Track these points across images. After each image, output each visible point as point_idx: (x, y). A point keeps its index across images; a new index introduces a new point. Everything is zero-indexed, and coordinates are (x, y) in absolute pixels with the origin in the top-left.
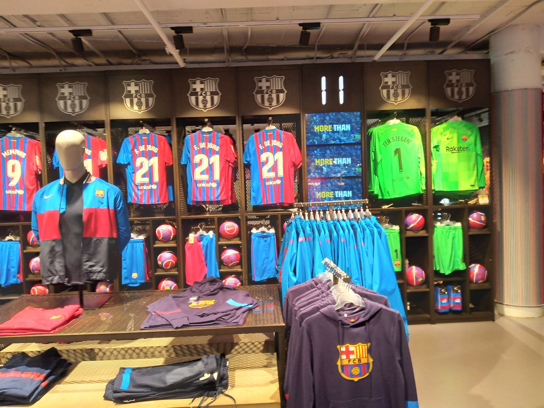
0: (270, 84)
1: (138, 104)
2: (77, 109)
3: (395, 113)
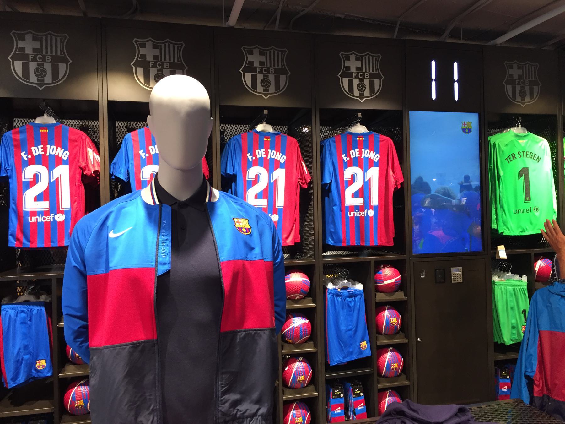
2: (48, 79)
3: (266, 112)
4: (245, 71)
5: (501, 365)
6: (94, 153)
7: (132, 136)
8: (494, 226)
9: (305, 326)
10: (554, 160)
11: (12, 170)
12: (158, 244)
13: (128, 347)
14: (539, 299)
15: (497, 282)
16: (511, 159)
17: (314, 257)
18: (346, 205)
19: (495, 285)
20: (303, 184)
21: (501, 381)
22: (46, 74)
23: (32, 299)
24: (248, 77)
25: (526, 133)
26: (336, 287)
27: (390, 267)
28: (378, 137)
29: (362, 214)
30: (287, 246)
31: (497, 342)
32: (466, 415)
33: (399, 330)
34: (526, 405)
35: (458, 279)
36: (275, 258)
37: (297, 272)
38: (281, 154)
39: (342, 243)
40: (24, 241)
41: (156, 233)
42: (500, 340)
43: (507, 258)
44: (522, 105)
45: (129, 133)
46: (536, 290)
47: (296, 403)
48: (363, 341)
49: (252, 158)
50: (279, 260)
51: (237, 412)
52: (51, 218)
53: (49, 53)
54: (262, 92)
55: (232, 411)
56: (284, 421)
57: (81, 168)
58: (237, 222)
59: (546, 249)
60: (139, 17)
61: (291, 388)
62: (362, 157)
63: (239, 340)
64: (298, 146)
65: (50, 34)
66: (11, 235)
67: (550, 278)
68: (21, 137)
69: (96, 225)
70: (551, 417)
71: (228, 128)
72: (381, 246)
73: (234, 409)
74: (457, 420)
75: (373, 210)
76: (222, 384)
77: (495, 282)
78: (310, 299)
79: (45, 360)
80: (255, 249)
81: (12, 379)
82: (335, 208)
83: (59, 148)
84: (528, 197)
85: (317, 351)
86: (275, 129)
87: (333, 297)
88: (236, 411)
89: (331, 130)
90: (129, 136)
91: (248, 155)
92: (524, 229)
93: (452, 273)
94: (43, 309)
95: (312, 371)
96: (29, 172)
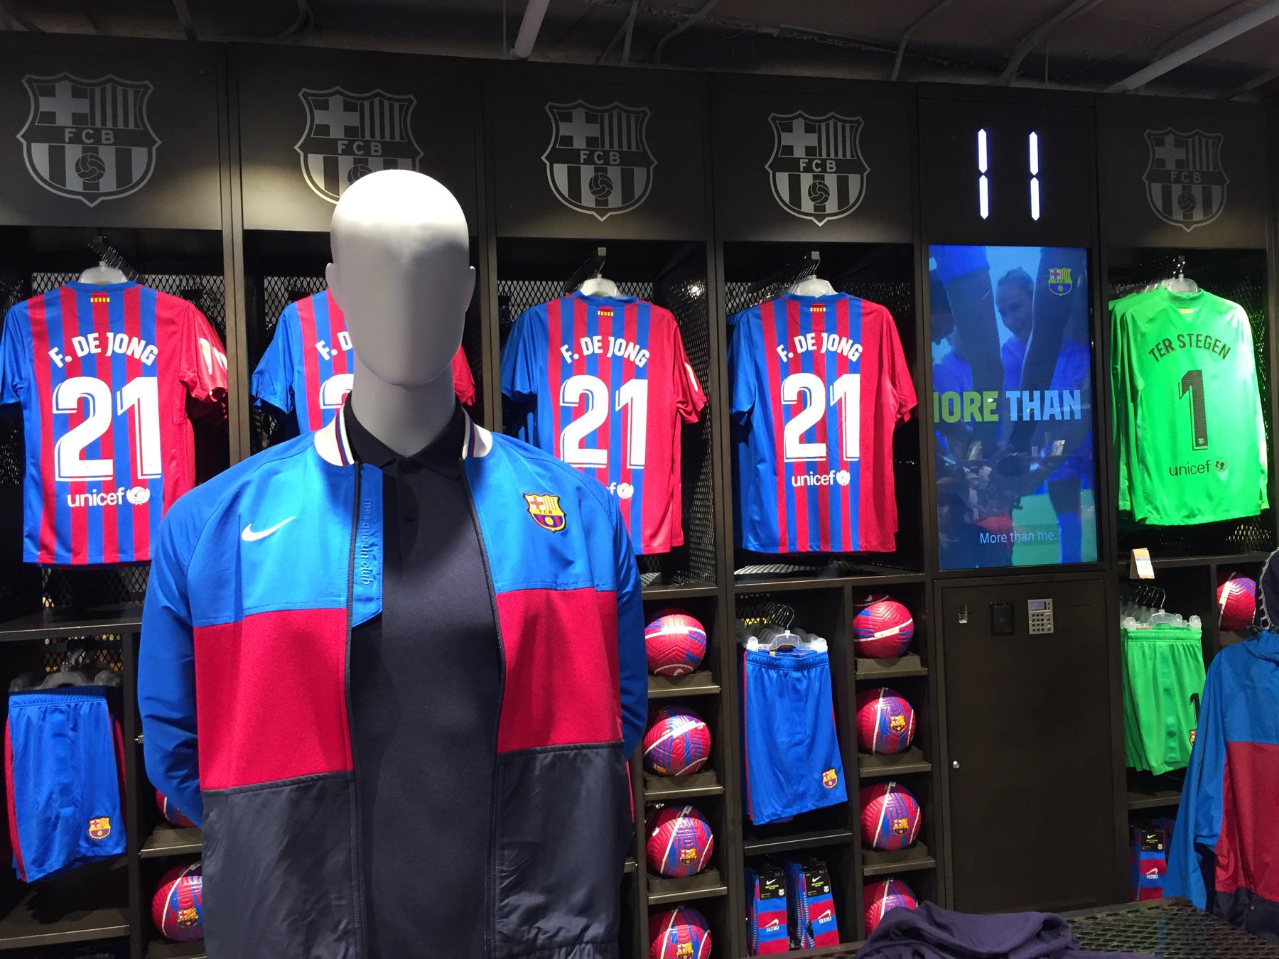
0: (1187, 152)
1: (86, 168)
2: (108, 183)
3: (602, 251)
4: (554, 158)
5: (1142, 819)
6: (215, 351)
7: (299, 310)
8: (1124, 504)
9: (696, 736)
10: (1260, 353)
11: (29, 389)
12: (354, 554)
13: (287, 789)
14: (1227, 671)
15: (1133, 632)
16: (1162, 353)
17: (716, 578)
18: (786, 461)
19: (1129, 638)
20: (689, 413)
21: (1144, 856)
22: (104, 171)
23: (78, 680)
24: (560, 174)
25: (1196, 291)
26: (766, 647)
27: (887, 600)
28: (857, 305)
29: (823, 480)
30: (654, 555)
31: (1134, 769)
32: (1059, 935)
33: (911, 743)
34: (1198, 911)
35: (1043, 625)
36: (620, 583)
37: (675, 613)
38: (638, 347)
39: (779, 548)
40: (58, 548)
41: (349, 531)
42: (1141, 763)
43: (1155, 576)
44: (1185, 229)
45: (292, 302)
46: (1221, 648)
47: (677, 910)
48: (827, 768)
49: (571, 357)
50: (629, 588)
51: (537, 934)
52: (117, 496)
53: (109, 124)
54: (593, 206)
55: (526, 932)
56: (651, 952)
57: (184, 384)
58: (533, 503)
59: (1243, 555)
60: (314, 41)
61: (665, 876)
62: (823, 351)
63: (541, 770)
64: (676, 328)
65: (378, 94)
66: (27, 536)
67: (1253, 622)
68: (49, 314)
69: (213, 514)
70: (1253, 939)
71: (518, 288)
72: (868, 552)
73: (531, 926)
74: (1038, 948)
75: (847, 471)
76: (502, 871)
77: (1128, 633)
78: (708, 674)
79: (108, 819)
80: (573, 565)
81: (34, 862)
82: (761, 467)
83: (135, 340)
84: (1201, 438)
85: (724, 792)
86: (624, 289)
87: (760, 670)
88: (534, 931)
89: (751, 291)
90: (293, 310)
91: (563, 349)
92: (1193, 511)
93: (1031, 612)
94: (104, 703)
95: (713, 838)
96: (67, 394)
